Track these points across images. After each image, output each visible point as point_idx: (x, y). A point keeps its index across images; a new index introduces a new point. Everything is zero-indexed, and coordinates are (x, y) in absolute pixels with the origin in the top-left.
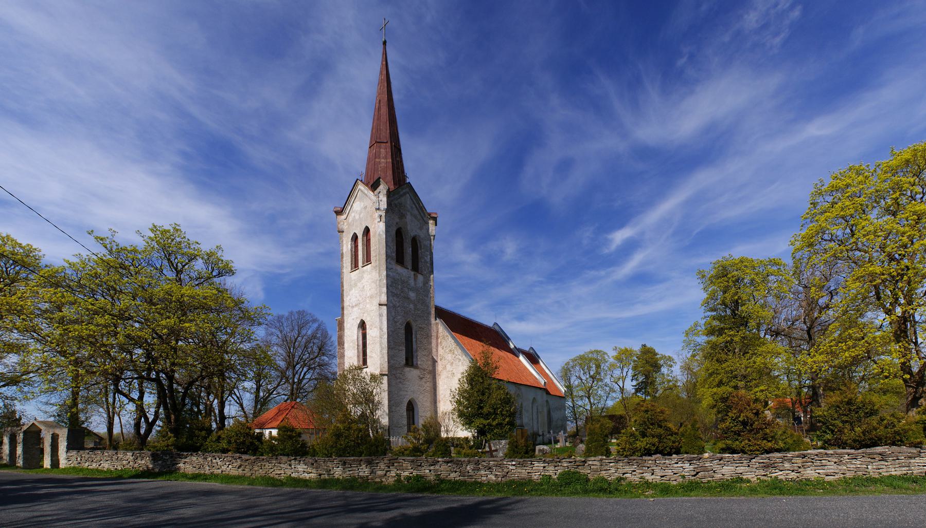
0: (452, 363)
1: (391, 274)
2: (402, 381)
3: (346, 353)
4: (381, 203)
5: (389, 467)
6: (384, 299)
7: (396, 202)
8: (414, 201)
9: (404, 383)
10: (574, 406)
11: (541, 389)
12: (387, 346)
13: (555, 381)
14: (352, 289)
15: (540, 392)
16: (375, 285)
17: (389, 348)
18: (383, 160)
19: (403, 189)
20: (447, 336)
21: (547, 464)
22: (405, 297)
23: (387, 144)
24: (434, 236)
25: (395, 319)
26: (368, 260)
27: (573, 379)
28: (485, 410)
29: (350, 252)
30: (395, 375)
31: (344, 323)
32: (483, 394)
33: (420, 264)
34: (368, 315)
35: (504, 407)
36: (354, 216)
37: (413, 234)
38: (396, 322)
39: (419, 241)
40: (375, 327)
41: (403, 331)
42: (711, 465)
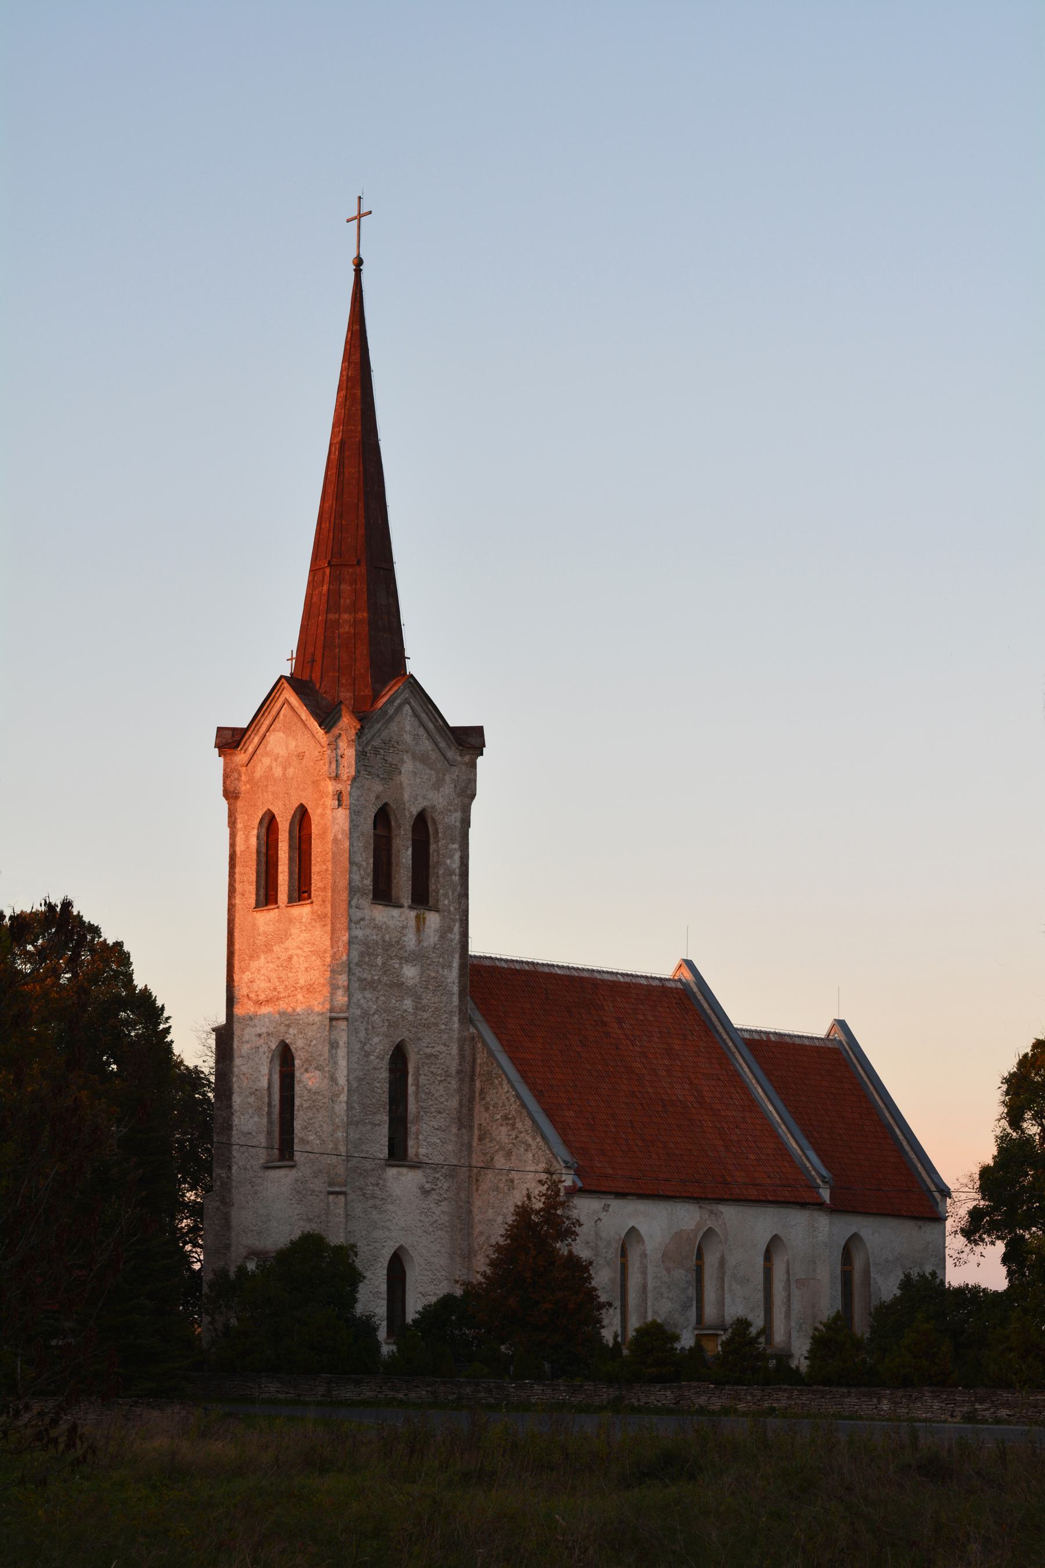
2: (378, 1203)
3: (236, 1121)
4: (344, 762)
5: (381, 1388)
14: (258, 957)
16: (319, 962)
21: (545, 1388)
25: (367, 1048)
26: (301, 892)
29: (255, 856)
30: (361, 1189)
33: (432, 880)
39: (433, 819)
40: (317, 1068)
41: (384, 1075)
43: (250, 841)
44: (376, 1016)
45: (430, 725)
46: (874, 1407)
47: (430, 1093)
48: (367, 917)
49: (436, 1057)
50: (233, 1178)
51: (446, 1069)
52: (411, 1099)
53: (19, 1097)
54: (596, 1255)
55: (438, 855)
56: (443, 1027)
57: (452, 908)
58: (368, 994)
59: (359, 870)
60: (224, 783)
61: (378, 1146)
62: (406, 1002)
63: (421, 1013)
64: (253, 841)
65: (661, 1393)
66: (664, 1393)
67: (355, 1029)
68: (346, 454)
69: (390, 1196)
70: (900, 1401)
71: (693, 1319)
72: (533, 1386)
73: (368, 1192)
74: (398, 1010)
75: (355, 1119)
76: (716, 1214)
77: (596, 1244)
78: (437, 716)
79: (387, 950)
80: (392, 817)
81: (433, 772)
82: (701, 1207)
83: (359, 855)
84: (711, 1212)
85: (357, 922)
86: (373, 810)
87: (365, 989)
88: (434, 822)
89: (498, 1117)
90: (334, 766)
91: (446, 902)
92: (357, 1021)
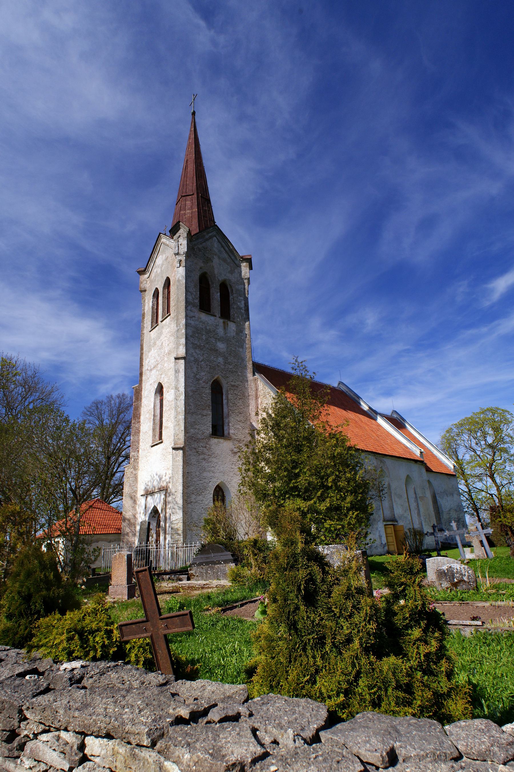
1: (193, 323)
6: (182, 351)
8: (223, 244)
9: (210, 460)
10: (470, 490)
11: (416, 461)
12: (184, 409)
13: (435, 452)
15: (416, 467)
17: (188, 412)
18: (188, 211)
19: (208, 233)
20: (269, 393)
22: (211, 350)
23: (193, 196)
24: (249, 279)
25: (197, 376)
27: (461, 452)
28: (302, 481)
29: (151, 310)
30: (195, 449)
31: (141, 391)
32: (299, 450)
35: (340, 472)
36: (157, 272)
37: (221, 278)
38: (198, 380)
41: (208, 391)
44: (203, 362)
47: (234, 403)
48: (196, 316)
49: (237, 387)
50: (140, 456)
52: (225, 407)
53: (21, 662)
56: (240, 374)
64: (151, 304)
69: (214, 453)
71: (382, 516)
80: (210, 280)
84: (381, 461)
85: (191, 317)
87: (196, 349)
88: (231, 286)
90: (177, 248)
92: (191, 362)
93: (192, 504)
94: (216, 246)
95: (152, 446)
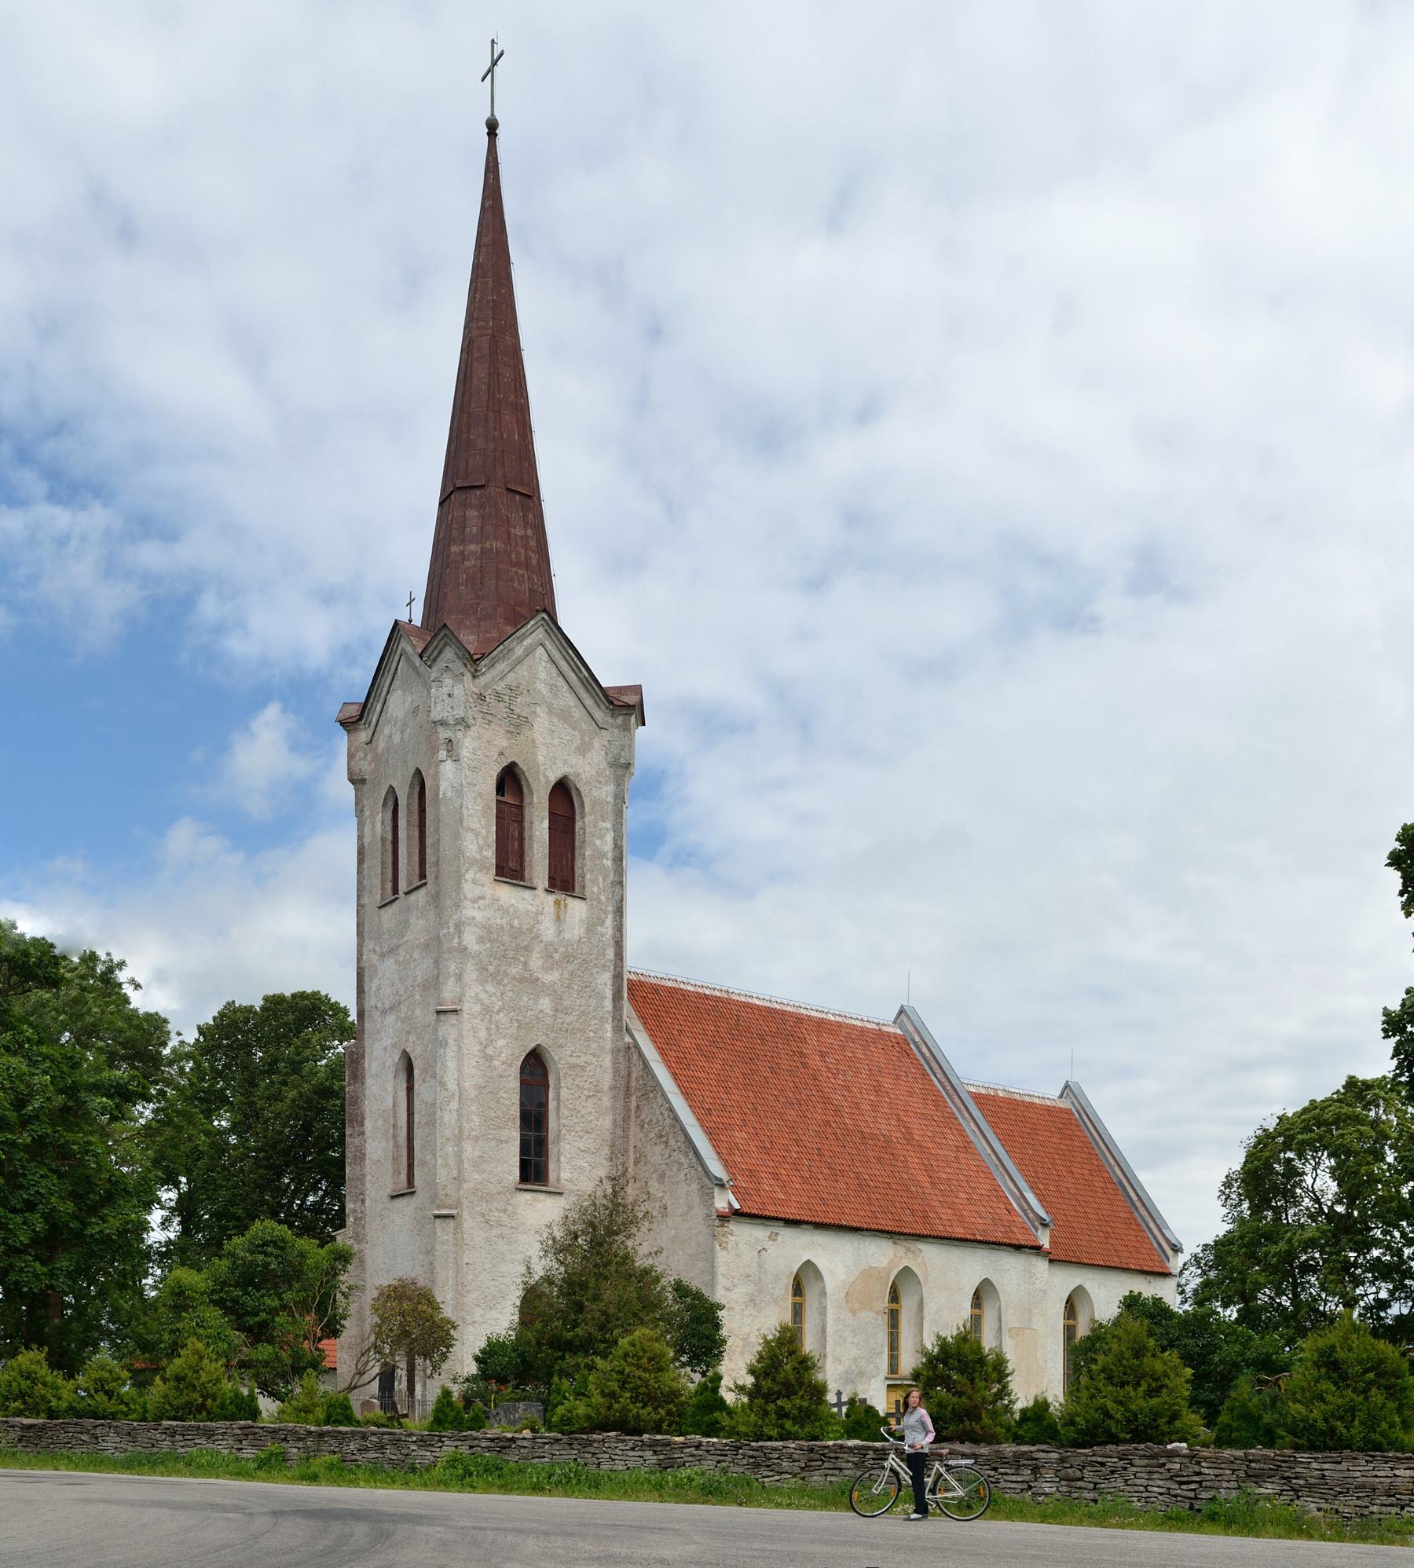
0: (663, 1176)
2: (505, 1231)
5: (240, 1441)
7: (502, 685)
21: (460, 1443)
25: (490, 1051)
30: (483, 1215)
31: (364, 1057)
34: (418, 1039)
36: (390, 736)
39: (577, 789)
42: (682, 1455)
43: (379, 824)
44: (502, 1015)
45: (572, 677)
46: (1025, 1486)
47: (574, 1109)
48: (488, 896)
49: (583, 1068)
50: (367, 1212)
51: (595, 1083)
54: (760, 1291)
55: (584, 834)
56: (592, 1034)
57: (603, 898)
58: (490, 988)
59: (477, 839)
60: (349, 764)
61: (505, 1165)
62: (542, 1001)
63: (563, 1016)
65: (635, 1453)
66: (640, 1453)
67: (473, 1027)
68: (475, 356)
70: (1078, 1474)
72: (443, 1439)
73: (492, 1218)
74: (532, 1010)
75: (474, 1133)
76: (914, 1252)
77: (760, 1278)
78: (580, 665)
79: (516, 938)
81: (576, 733)
82: (895, 1243)
83: (476, 819)
86: (495, 768)
87: (486, 981)
89: (653, 1135)
91: (595, 889)
93: (476, 1325)
94: (542, 676)
95: (393, 1197)
